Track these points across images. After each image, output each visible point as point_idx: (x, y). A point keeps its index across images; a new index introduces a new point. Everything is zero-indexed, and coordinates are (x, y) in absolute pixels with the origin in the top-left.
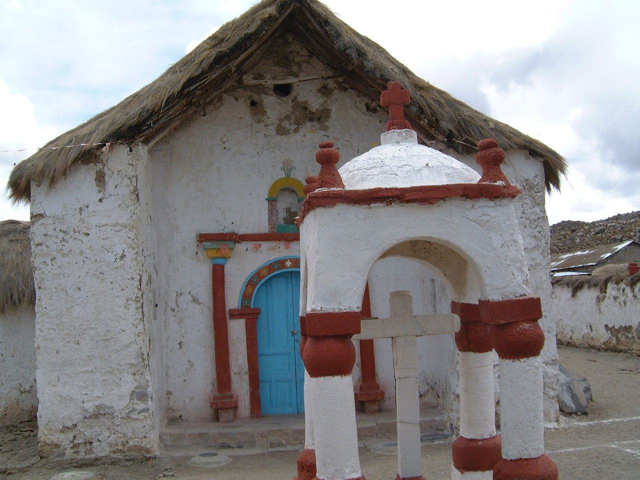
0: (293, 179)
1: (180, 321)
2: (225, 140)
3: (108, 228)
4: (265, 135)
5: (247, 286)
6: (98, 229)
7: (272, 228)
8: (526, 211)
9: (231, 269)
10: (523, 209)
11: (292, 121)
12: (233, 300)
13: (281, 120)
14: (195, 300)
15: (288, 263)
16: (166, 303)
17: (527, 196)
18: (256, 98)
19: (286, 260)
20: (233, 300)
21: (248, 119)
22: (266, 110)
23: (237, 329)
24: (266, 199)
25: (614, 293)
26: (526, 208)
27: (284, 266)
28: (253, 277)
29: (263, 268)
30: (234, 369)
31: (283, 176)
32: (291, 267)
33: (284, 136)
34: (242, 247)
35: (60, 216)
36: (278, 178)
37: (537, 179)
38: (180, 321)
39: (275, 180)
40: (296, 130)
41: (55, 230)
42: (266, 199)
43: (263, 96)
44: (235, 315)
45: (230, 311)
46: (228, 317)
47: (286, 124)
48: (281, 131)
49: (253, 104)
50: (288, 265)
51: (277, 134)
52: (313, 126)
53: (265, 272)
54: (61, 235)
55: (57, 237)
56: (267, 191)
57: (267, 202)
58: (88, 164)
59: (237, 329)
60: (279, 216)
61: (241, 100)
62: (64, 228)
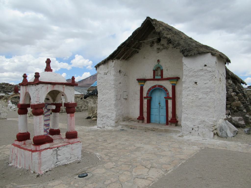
9: (144, 87)
20: (145, 95)
23: (145, 101)
32: (158, 87)
46: (143, 99)
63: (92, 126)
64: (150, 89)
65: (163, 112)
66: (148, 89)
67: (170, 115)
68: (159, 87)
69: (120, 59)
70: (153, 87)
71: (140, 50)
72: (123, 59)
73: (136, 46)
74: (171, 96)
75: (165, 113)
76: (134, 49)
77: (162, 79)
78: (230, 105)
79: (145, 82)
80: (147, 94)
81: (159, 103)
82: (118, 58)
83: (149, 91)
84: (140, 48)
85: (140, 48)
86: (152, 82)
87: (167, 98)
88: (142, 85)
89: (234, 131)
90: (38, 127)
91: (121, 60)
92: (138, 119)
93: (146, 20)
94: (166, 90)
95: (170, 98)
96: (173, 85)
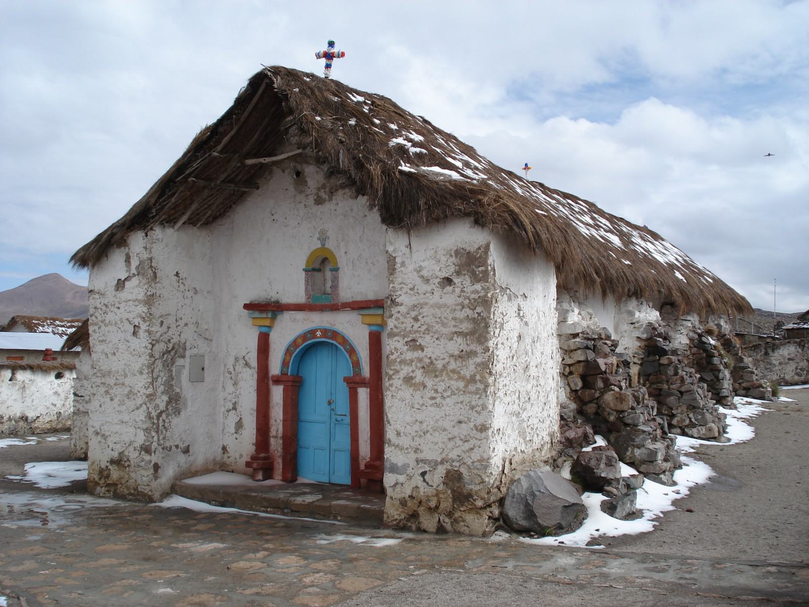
0: (327, 249)
1: (235, 384)
2: (273, 213)
3: (131, 303)
4: (305, 205)
5: (285, 354)
6: (125, 303)
7: (308, 298)
8: (465, 289)
9: (274, 336)
10: (462, 286)
11: (327, 190)
12: (275, 368)
13: (319, 189)
14: (247, 364)
15: (319, 333)
16: (225, 365)
17: (466, 272)
18: (299, 167)
19: (316, 330)
20: (275, 368)
21: (292, 189)
22: (307, 179)
23: (277, 393)
24: (304, 270)
25: (141, 392)
26: (465, 286)
27: (315, 337)
28: (290, 346)
29: (299, 337)
30: (273, 432)
31: (319, 246)
32: (321, 337)
33: (320, 206)
34: (287, 316)
35: (103, 293)
36: (314, 248)
37: (480, 251)
38: (235, 384)
39: (312, 251)
40: (330, 199)
41: (100, 303)
42: (304, 270)
43: (305, 166)
44: (277, 381)
45: (273, 376)
46: (271, 382)
47: (323, 194)
48: (319, 201)
49: (298, 174)
50: (318, 335)
51: (315, 204)
52: (344, 194)
53: (300, 341)
54: (104, 308)
55: (101, 309)
56: (305, 262)
57: (304, 272)
58: (120, 248)
59: (277, 393)
60: (326, 285)
61: (287, 172)
62: (106, 302)
63: (235, 487)
64: (294, 344)
65: (343, 439)
66: (339, 328)
67: (365, 450)
68: (325, 338)
69: (176, 227)
70: (304, 336)
71: (258, 188)
72: (192, 222)
73: (236, 176)
74: (366, 371)
75: (349, 440)
76: (232, 186)
77: (335, 308)
78: (597, 403)
79: (274, 318)
80: (285, 364)
81: (330, 403)
82: (170, 221)
83: (288, 352)
84: (259, 181)
85: (259, 181)
86: (299, 315)
87: (353, 384)
88: (264, 330)
89: (565, 507)
90: (186, 325)
91: (180, 227)
92: (248, 464)
93: (109, 232)
94: (352, 351)
95: (363, 383)
96: (374, 328)
